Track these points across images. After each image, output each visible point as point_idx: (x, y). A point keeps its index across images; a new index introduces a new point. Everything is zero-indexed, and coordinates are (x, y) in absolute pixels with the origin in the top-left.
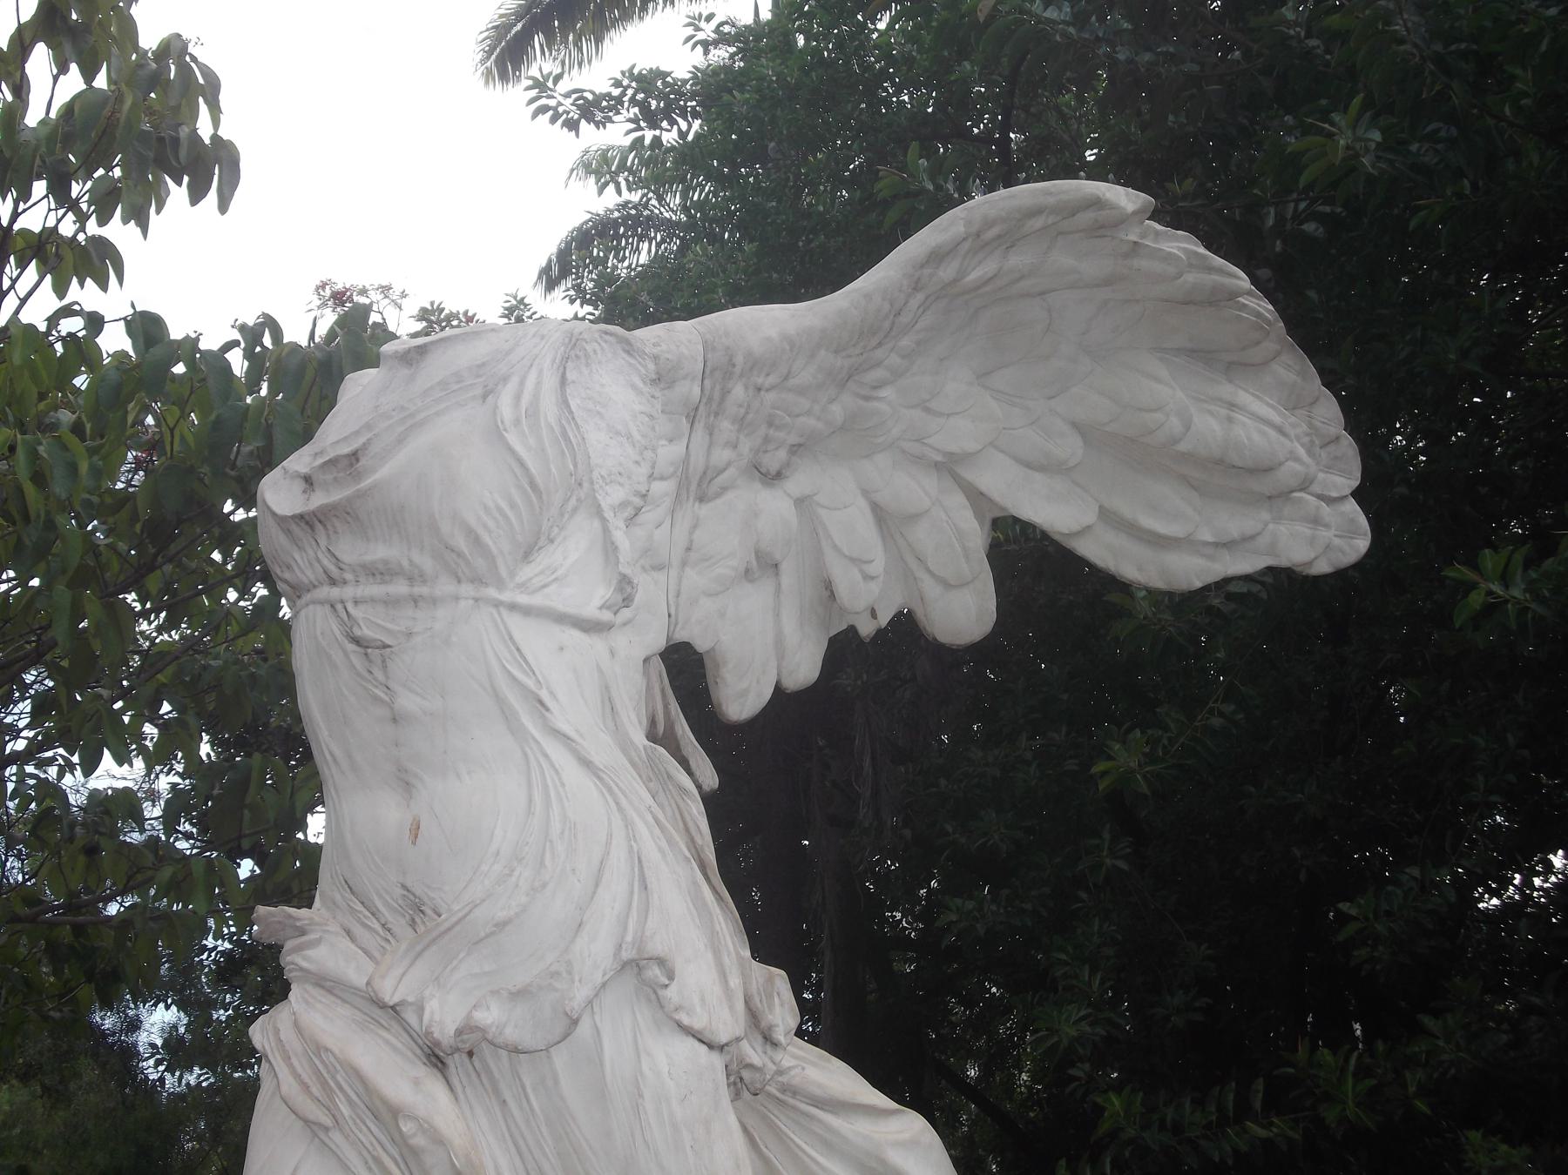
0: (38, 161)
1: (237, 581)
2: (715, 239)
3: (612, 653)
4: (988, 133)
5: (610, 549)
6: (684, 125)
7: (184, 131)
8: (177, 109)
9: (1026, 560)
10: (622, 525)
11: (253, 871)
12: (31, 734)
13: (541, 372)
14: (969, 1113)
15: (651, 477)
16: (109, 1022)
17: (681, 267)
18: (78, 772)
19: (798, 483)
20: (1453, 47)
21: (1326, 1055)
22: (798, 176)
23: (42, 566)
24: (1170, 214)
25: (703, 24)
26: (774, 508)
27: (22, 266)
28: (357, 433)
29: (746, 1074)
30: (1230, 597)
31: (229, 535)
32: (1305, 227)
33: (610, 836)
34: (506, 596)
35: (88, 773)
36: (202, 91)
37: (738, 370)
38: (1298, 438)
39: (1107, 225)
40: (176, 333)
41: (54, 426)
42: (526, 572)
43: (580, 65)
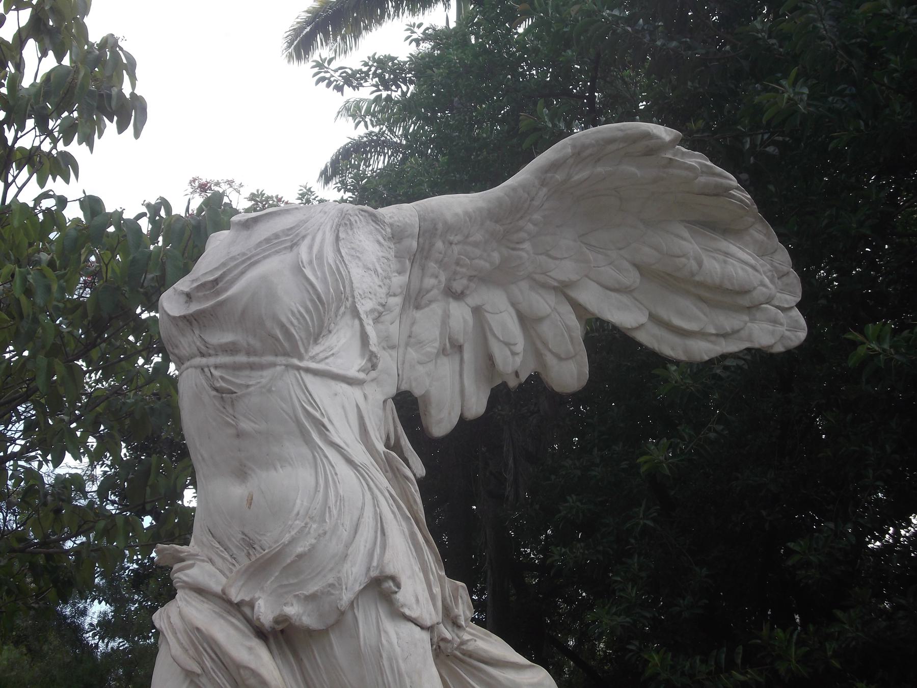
0: (29, 108)
1: (144, 353)
2: (423, 154)
3: (365, 397)
4: (582, 93)
5: (364, 339)
6: (404, 88)
7: (114, 91)
8: (110, 78)
9: (606, 343)
10: (371, 322)
11: (151, 523)
12: (23, 442)
13: (324, 233)
14: (569, 667)
15: (389, 295)
16: (68, 611)
17: (403, 170)
18: (50, 464)
19: (474, 300)
20: (854, 41)
21: (779, 633)
22: (471, 118)
23: (31, 345)
24: (693, 143)
25: (416, 29)
26: (460, 315)
27: (20, 169)
28: (216, 269)
29: (442, 644)
30: (726, 368)
31: (139, 326)
32: (767, 149)
33: (364, 504)
34: (303, 364)
35: (55, 466)
36: (125, 67)
37: (439, 232)
38: (765, 273)
39: (653, 149)
40: (109, 208)
41: (38, 262)
42: (315, 350)
43: (345, 53)
